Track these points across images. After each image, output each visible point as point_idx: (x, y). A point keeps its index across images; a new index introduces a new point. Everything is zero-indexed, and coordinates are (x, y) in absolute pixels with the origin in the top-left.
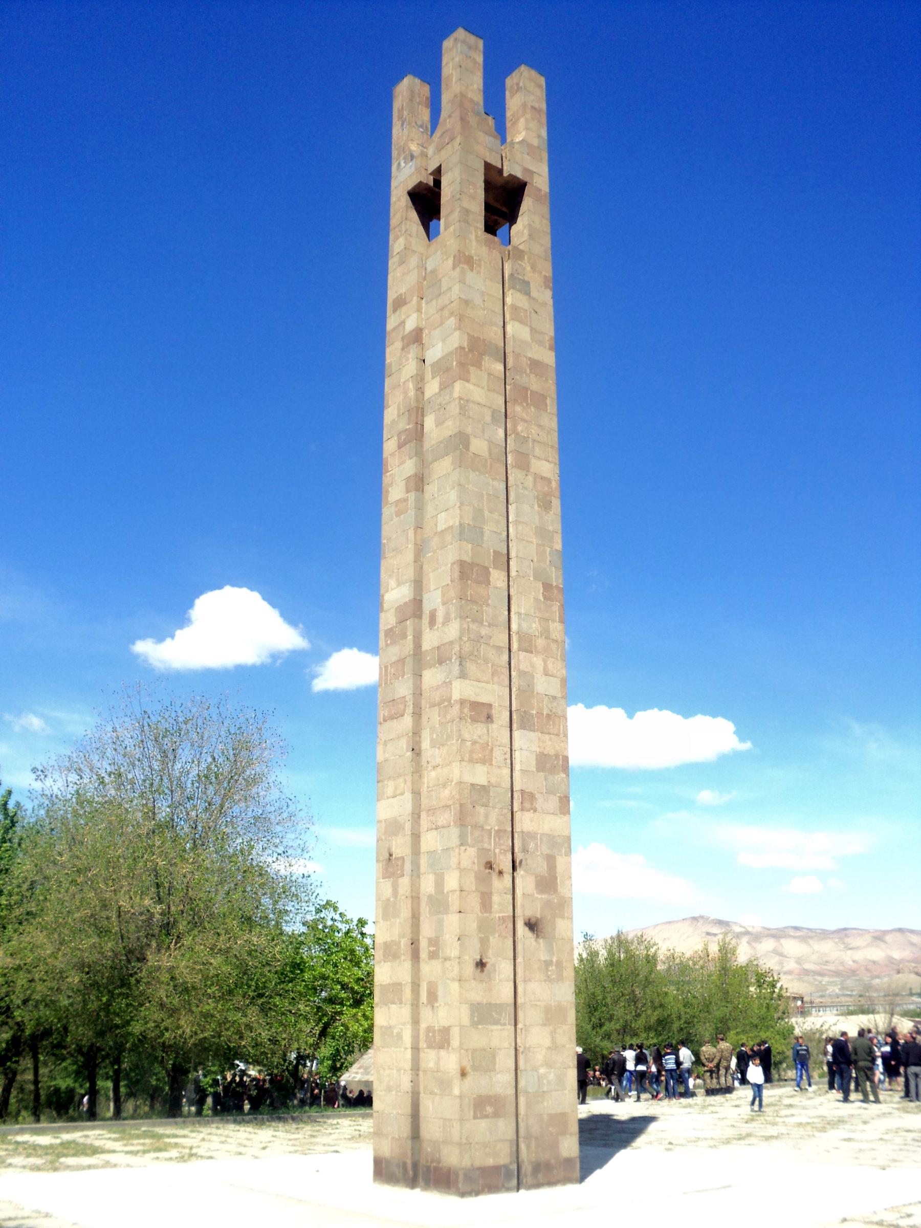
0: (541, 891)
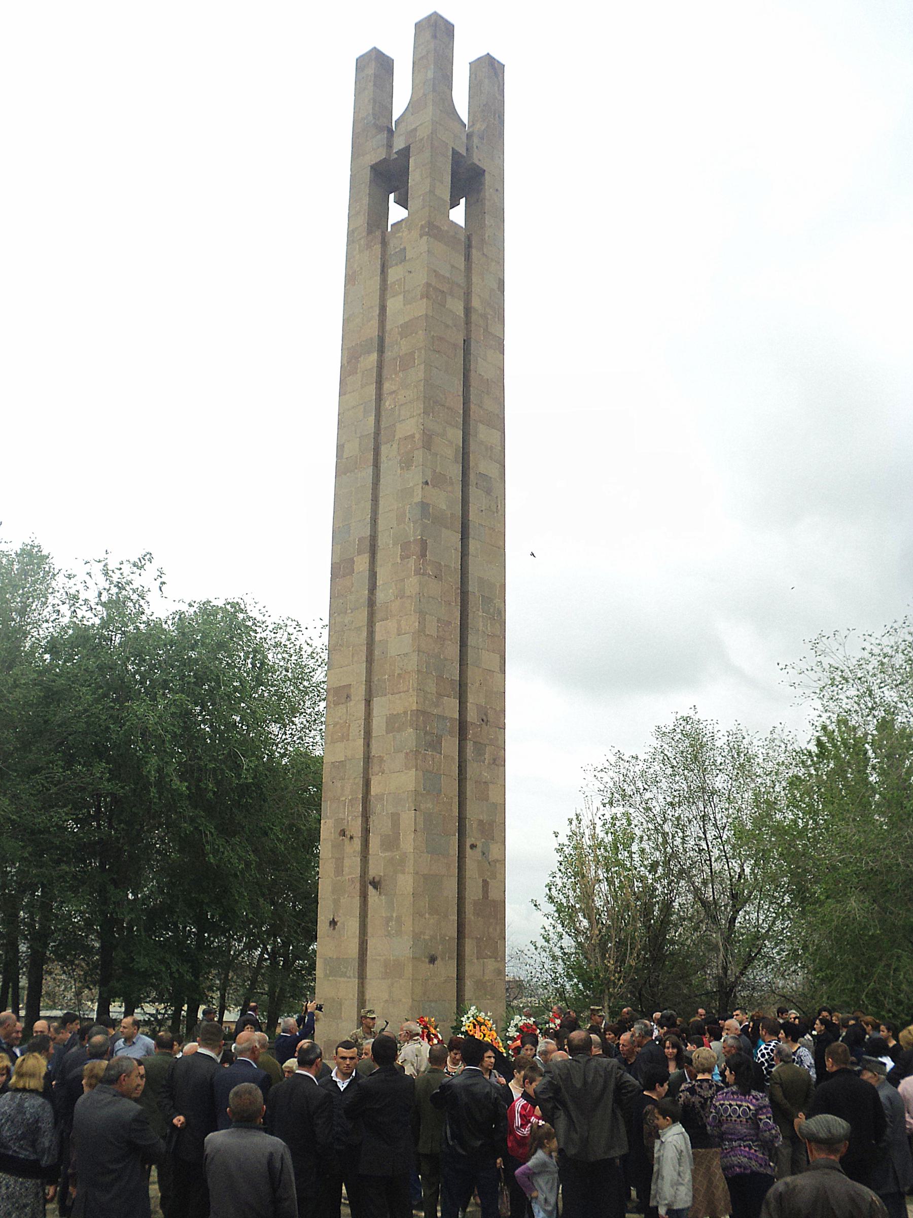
0: (386, 850)
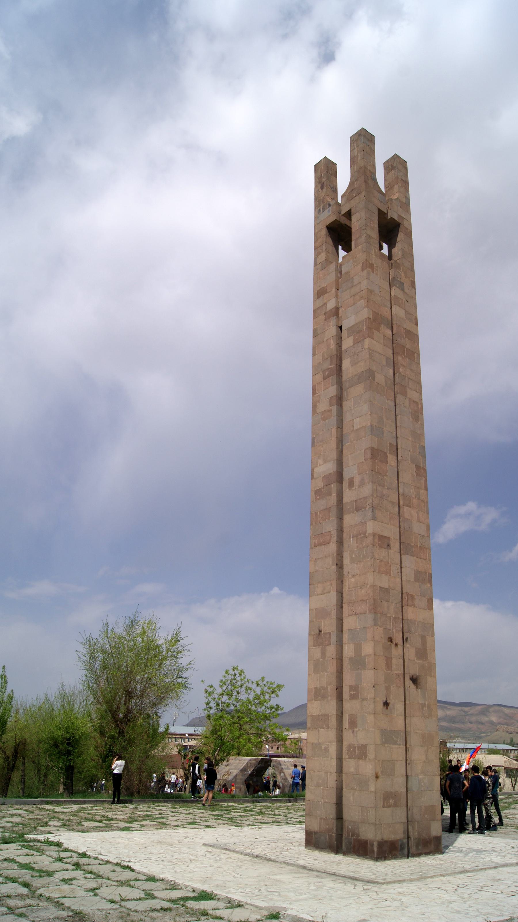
0: (419, 659)
